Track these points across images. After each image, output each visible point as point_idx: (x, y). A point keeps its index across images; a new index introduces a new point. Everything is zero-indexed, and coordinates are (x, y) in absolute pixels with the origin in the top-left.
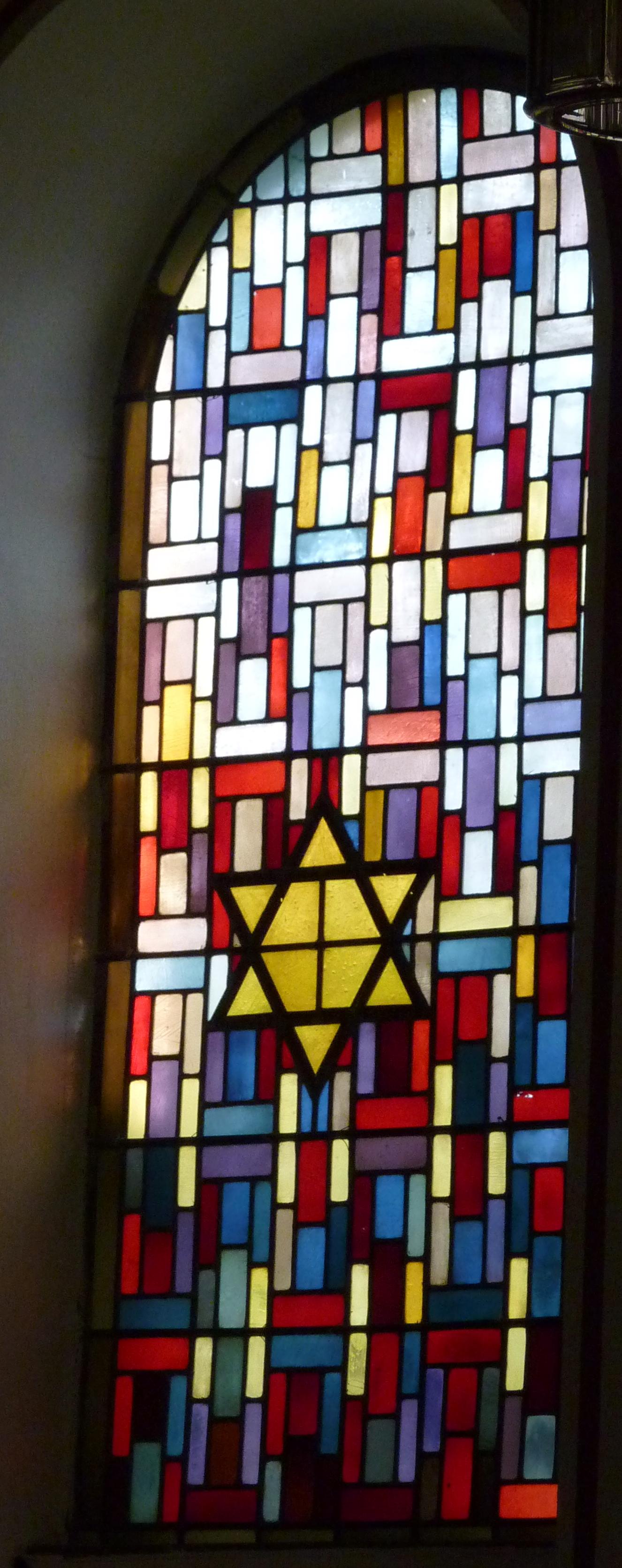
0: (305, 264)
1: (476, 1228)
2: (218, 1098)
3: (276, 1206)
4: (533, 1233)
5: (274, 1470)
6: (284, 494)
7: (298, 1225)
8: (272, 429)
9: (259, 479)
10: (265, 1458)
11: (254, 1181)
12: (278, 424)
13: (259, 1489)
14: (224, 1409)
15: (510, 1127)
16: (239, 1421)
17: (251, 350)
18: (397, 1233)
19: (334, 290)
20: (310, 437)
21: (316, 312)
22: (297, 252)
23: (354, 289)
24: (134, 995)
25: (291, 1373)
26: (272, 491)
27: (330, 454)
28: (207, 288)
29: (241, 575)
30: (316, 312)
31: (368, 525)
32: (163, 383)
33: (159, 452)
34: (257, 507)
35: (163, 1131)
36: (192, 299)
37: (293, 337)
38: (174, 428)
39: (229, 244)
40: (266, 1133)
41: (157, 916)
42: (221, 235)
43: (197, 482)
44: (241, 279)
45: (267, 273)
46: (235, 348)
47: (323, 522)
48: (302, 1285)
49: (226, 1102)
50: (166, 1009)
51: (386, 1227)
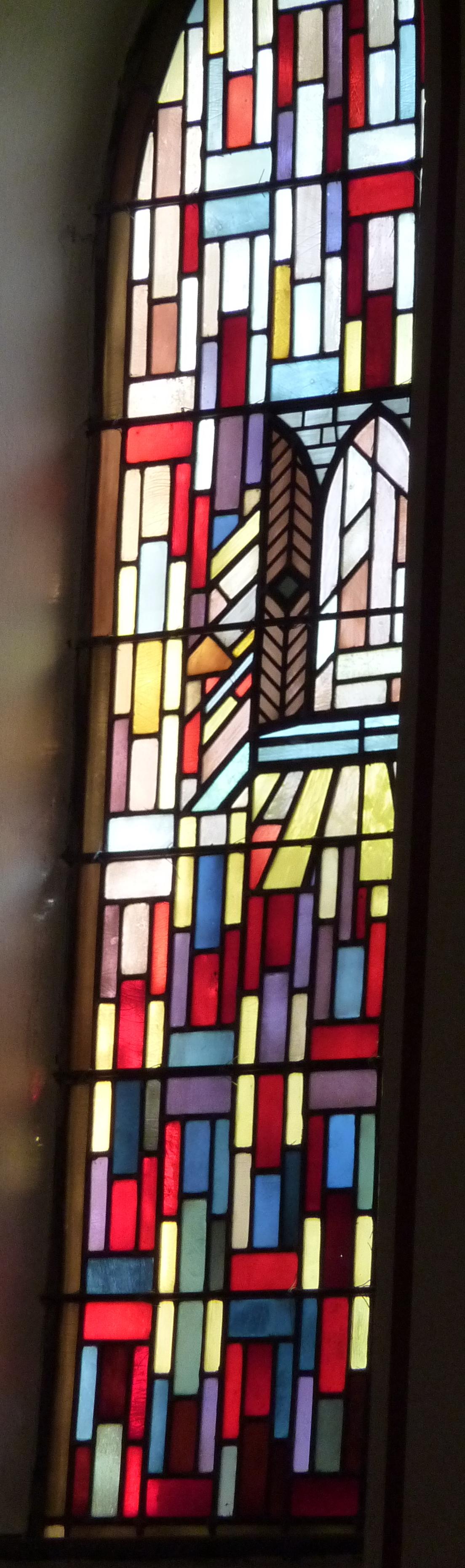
0: (275, 45)
1: (130, 1186)
2: (181, 1023)
3: (234, 1151)
4: (183, 1197)
5: (230, 1454)
6: (259, 321)
7: (256, 1172)
8: (390, 220)
9: (234, 303)
10: (221, 1442)
11: (212, 1118)
12: (395, 214)
13: (214, 1477)
14: (186, 1385)
15: (307, 1067)
16: (197, 1400)
17: (226, 149)
18: (347, 1183)
19: (301, 77)
20: (283, 253)
21: (285, 104)
22: (267, 33)
23: (319, 74)
24: (103, 903)
25: (247, 1343)
26: (246, 315)
27: (301, 272)
28: (184, 80)
29: (218, 414)
30: (285, 104)
31: (340, 354)
32: (144, 192)
33: (140, 271)
34: (234, 331)
35: (273, 1057)
36: (170, 91)
37: (264, 134)
38: (153, 242)
39: (205, 25)
40: (224, 1063)
41: (127, 813)
42: (195, 15)
43: (318, 285)
44: (216, 66)
45: (239, 61)
46: (210, 147)
47: (297, 353)
48: (258, 1243)
49: (190, 1027)
50: (136, 920)
51: (338, 1176)
